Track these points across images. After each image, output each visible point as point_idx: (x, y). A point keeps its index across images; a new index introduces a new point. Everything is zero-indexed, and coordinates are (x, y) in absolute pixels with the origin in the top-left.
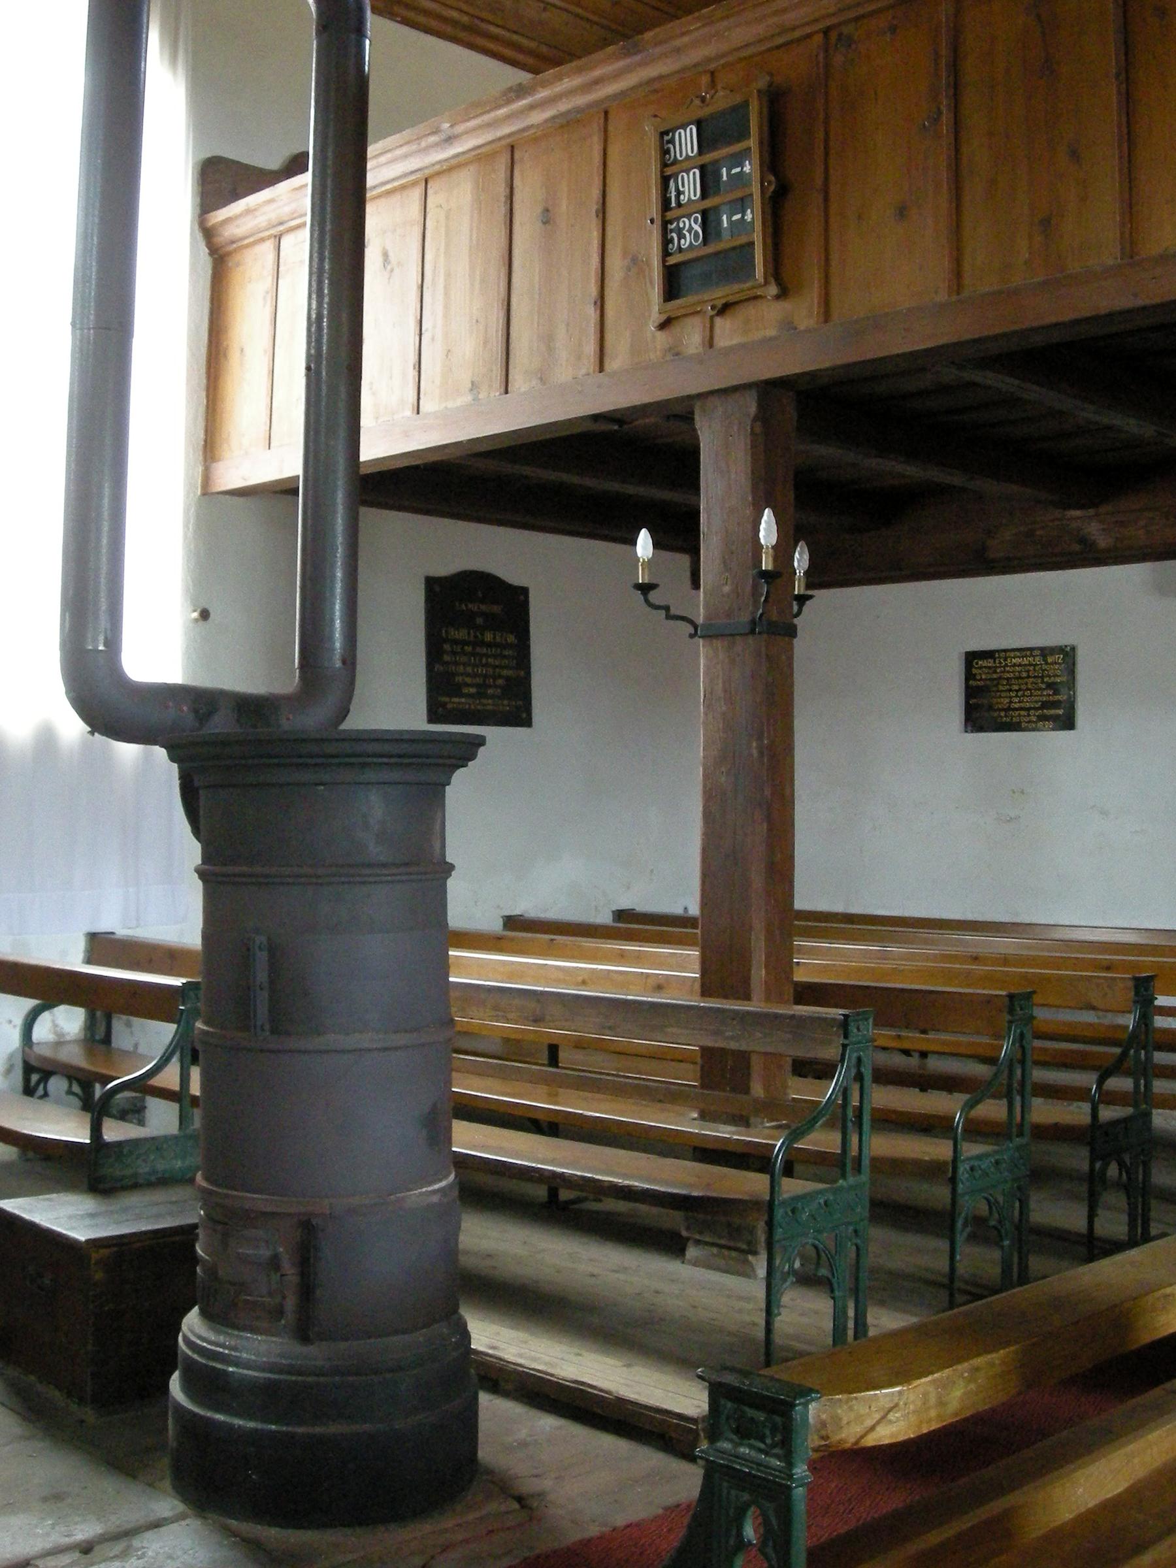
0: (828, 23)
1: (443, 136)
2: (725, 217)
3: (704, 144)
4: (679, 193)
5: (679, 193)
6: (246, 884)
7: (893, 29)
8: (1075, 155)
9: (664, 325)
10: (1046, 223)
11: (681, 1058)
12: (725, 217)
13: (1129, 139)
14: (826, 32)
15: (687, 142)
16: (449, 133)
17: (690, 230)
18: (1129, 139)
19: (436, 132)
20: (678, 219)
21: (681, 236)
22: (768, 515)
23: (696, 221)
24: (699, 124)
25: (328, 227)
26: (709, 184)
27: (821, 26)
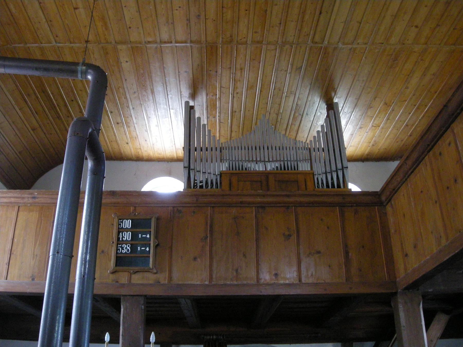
0: (175, 205)
1: (33, 196)
2: (139, 248)
3: (134, 225)
4: (123, 237)
5: (123, 237)
6: (411, 168)
7: (194, 212)
8: (244, 255)
9: (113, 272)
10: (237, 271)
11: (302, 168)
12: (139, 248)
13: (258, 247)
14: (173, 207)
15: (127, 224)
16: (36, 196)
17: (126, 248)
18: (258, 247)
19: (31, 194)
20: (122, 244)
21: (123, 249)
22: (153, 333)
23: (129, 246)
24: (132, 220)
25: (91, 230)
26: (134, 236)
27: (173, 205)
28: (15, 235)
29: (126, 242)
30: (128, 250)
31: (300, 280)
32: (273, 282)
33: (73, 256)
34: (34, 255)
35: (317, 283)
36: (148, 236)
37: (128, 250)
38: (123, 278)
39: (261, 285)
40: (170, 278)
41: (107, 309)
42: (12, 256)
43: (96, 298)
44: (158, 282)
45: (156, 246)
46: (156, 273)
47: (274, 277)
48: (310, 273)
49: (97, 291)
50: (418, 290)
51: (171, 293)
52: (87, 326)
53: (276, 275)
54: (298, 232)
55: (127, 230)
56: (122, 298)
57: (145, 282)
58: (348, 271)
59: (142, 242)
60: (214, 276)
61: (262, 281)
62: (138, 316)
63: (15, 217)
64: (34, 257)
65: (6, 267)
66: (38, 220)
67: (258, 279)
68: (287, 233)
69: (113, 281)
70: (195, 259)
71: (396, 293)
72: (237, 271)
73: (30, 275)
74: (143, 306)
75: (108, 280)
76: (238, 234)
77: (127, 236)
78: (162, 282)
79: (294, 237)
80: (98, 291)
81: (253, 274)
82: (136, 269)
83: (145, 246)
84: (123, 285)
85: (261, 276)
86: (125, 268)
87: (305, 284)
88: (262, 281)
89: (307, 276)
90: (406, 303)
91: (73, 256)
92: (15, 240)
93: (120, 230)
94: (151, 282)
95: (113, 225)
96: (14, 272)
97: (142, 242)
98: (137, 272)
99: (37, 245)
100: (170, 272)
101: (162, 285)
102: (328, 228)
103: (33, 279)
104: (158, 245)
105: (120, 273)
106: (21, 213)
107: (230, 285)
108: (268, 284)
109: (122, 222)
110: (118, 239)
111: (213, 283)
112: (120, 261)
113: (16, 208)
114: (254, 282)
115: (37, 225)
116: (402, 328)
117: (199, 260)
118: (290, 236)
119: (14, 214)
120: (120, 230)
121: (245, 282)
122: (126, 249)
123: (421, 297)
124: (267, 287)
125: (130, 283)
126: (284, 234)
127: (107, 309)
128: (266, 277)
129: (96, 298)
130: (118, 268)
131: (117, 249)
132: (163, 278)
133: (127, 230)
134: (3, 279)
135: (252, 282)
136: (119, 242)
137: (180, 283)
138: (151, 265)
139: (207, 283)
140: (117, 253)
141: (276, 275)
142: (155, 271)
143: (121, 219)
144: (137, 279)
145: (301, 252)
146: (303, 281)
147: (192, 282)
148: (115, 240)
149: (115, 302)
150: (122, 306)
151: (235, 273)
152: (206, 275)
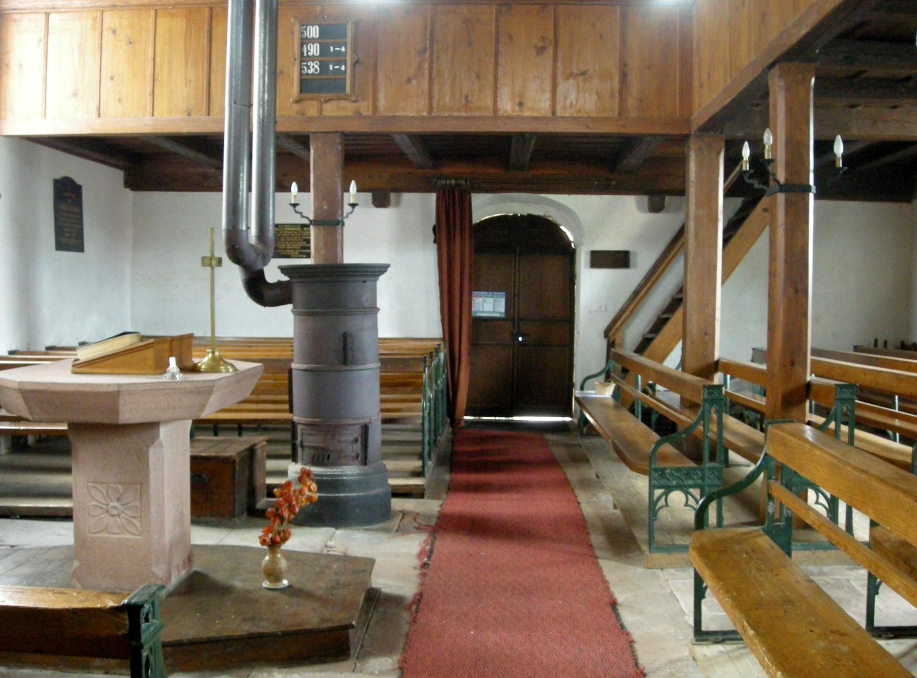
3: (324, 32)
4: (308, 51)
8: (478, 76)
15: (313, 32)
18: (496, 64)
21: (308, 68)
24: (320, 26)
26: (324, 50)
28: (157, 53)
29: (313, 58)
30: (316, 70)
31: (554, 113)
32: (515, 114)
33: (240, 435)
34: (186, 79)
35: (576, 118)
36: (343, 49)
37: (316, 70)
38: (312, 108)
39: (500, 118)
40: (375, 108)
41: (294, 148)
42: (156, 83)
43: (278, 136)
44: (358, 114)
45: (355, 63)
46: (356, 101)
47: (517, 108)
48: (568, 102)
49: (280, 128)
50: (722, 132)
51: (376, 128)
52: (271, 179)
53: (521, 104)
54: (556, 42)
55: (313, 41)
56: (311, 136)
57: (342, 114)
58: (622, 101)
59: (335, 59)
60: (435, 105)
61: (501, 113)
62: (334, 159)
63: (152, 26)
64: (186, 84)
65: (149, 99)
66: (186, 33)
67: (496, 110)
68: (540, 44)
69: (298, 113)
70: (409, 80)
71: (688, 136)
72: (467, 97)
73: (185, 109)
74: (339, 147)
75: (291, 115)
76: (470, 44)
77: (314, 50)
78: (364, 114)
79: (550, 50)
80: (282, 128)
81: (489, 102)
82: (328, 96)
83: (339, 63)
84: (311, 119)
85: (499, 105)
86: (315, 95)
87: (561, 117)
88: (501, 113)
89: (564, 108)
90: (700, 149)
91: (240, 435)
92: (158, 60)
93: (304, 41)
94: (350, 114)
95: (292, 33)
96: (162, 105)
97: (335, 59)
98: (330, 100)
99: (189, 65)
100: (375, 99)
101: (365, 117)
102: (601, 37)
103: (189, 115)
104: (357, 62)
105: (309, 102)
106: (159, 20)
107: (458, 118)
108: (509, 118)
109: (306, 29)
110: (302, 53)
111: (433, 114)
112: (307, 85)
113: (152, 13)
114: (489, 114)
115: (186, 38)
116: (691, 184)
117: (414, 82)
118: (543, 48)
119: (151, 20)
120: (304, 41)
121: (477, 114)
122: (313, 68)
123: (723, 144)
124: (507, 121)
125: (321, 116)
126: (536, 46)
127: (294, 148)
128: (507, 106)
129: (278, 136)
130: (304, 95)
131: (302, 69)
132: (365, 107)
133: (313, 41)
134: (148, 117)
135: (487, 114)
136: (304, 59)
137: (390, 114)
138: (348, 90)
139: (425, 114)
140: (301, 74)
141: (521, 104)
142: (354, 98)
143: (304, 24)
144: (330, 109)
145: (559, 72)
146: (558, 114)
147: (405, 114)
148: (297, 56)
149: (303, 140)
150: (312, 148)
151: (464, 102)
152: (423, 102)
